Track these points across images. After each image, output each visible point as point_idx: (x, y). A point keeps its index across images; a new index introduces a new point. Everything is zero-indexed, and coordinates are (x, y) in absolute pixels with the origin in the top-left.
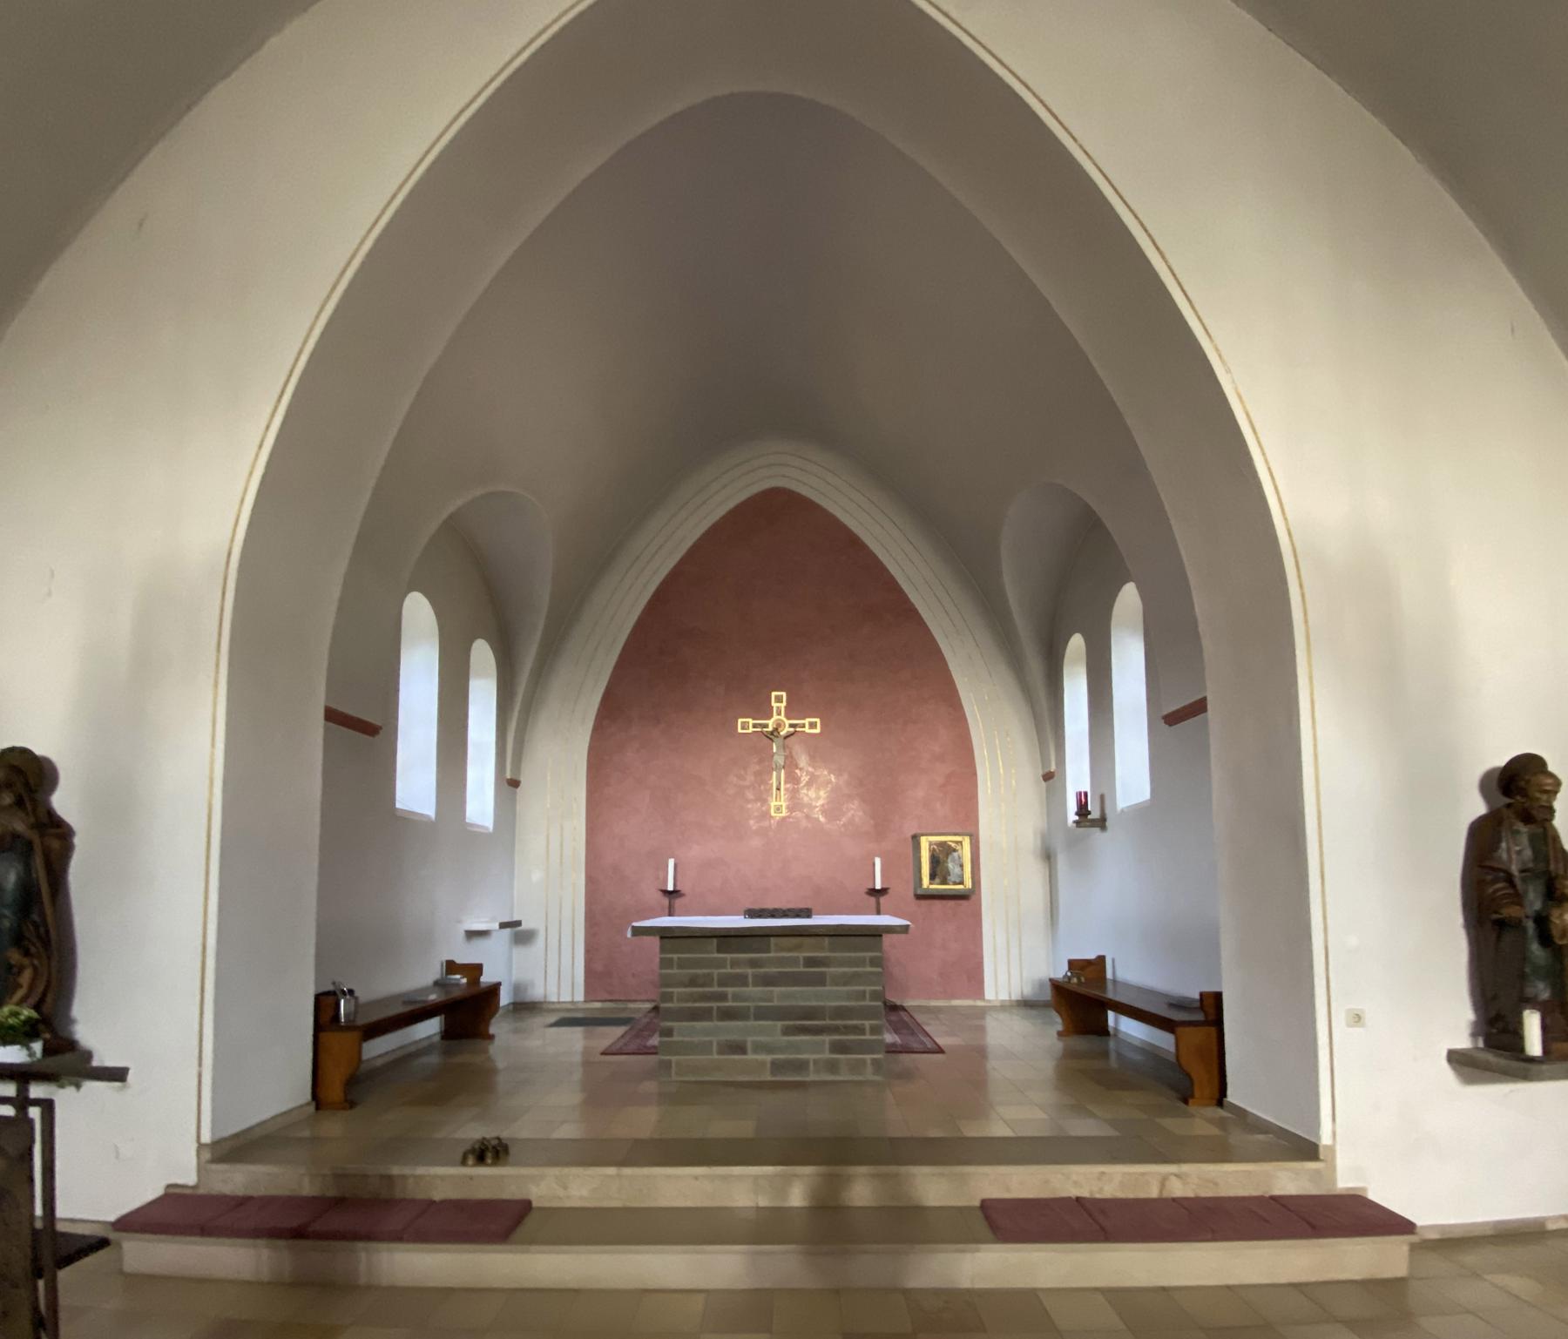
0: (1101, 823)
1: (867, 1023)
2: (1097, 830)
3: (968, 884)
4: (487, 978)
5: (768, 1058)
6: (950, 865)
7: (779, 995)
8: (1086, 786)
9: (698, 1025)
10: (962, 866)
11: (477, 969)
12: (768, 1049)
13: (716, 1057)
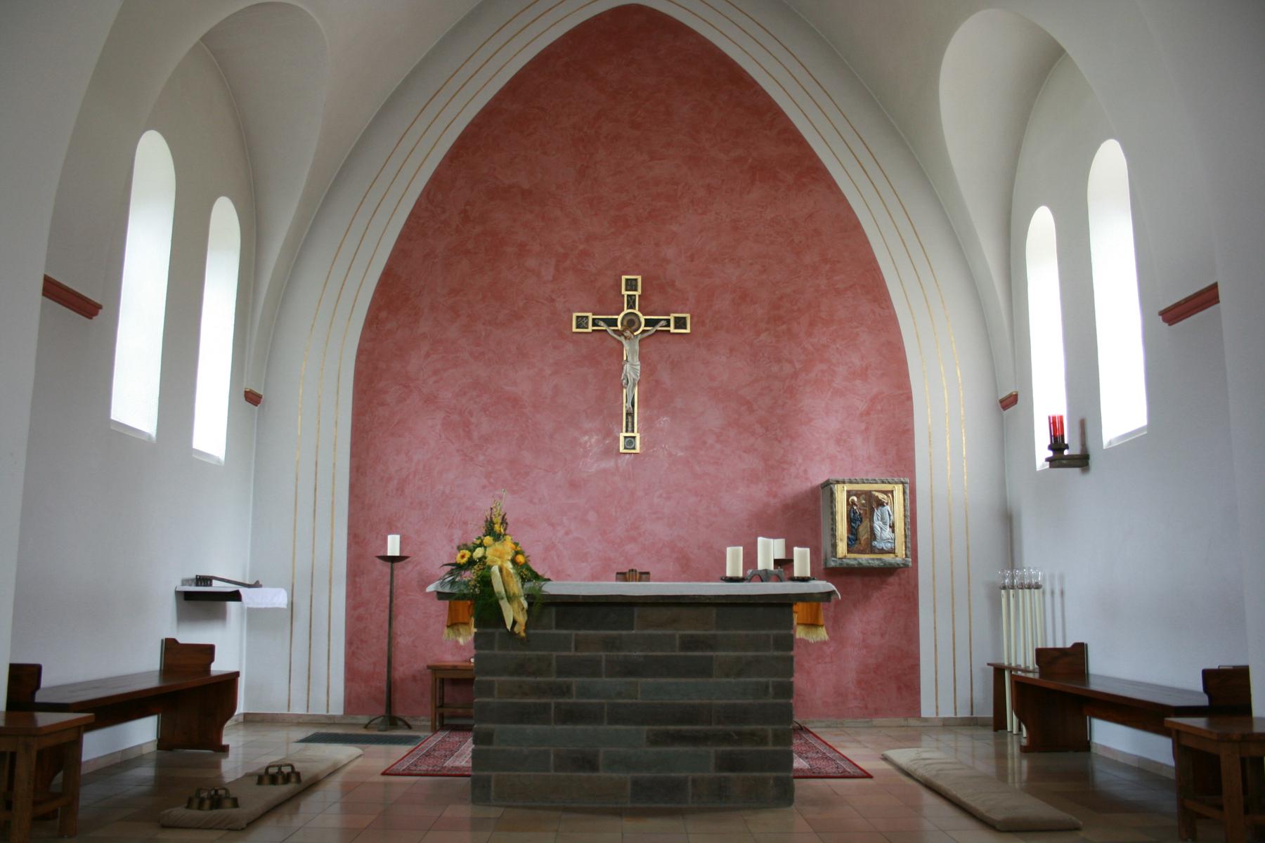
0: (1082, 461)
1: (769, 729)
2: (1076, 471)
3: (901, 550)
4: (220, 666)
5: (627, 776)
6: (877, 524)
7: (645, 690)
8: (1061, 409)
9: (529, 728)
10: (892, 527)
11: (208, 652)
13: (552, 773)
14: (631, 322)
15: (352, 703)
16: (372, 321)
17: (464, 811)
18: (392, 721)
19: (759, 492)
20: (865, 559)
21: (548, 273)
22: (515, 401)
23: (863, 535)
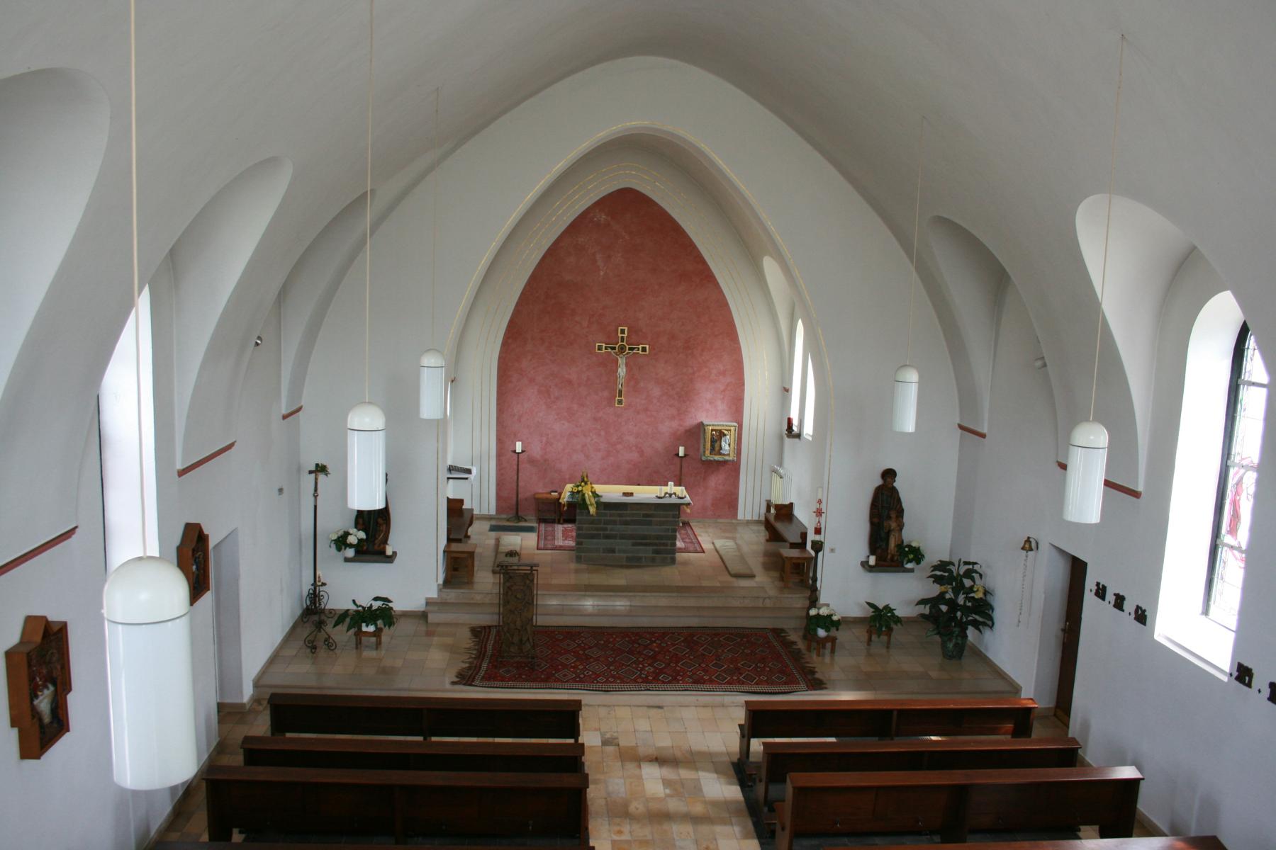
7: (630, 529)
12: (625, 552)
14: (622, 349)
15: (499, 509)
16: (505, 344)
17: (573, 566)
18: (518, 518)
19: (675, 424)
20: (717, 458)
21: (585, 324)
22: (570, 382)
23: (717, 445)
